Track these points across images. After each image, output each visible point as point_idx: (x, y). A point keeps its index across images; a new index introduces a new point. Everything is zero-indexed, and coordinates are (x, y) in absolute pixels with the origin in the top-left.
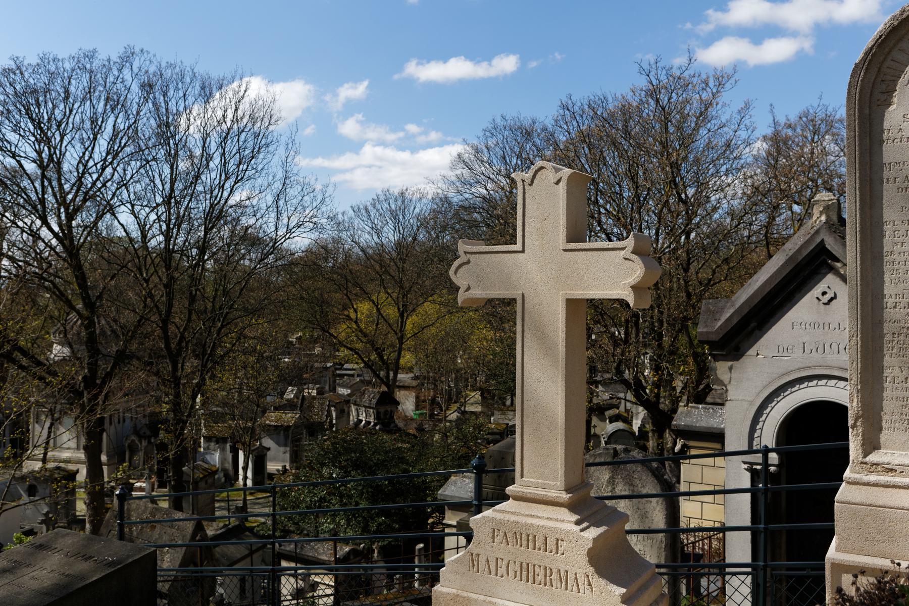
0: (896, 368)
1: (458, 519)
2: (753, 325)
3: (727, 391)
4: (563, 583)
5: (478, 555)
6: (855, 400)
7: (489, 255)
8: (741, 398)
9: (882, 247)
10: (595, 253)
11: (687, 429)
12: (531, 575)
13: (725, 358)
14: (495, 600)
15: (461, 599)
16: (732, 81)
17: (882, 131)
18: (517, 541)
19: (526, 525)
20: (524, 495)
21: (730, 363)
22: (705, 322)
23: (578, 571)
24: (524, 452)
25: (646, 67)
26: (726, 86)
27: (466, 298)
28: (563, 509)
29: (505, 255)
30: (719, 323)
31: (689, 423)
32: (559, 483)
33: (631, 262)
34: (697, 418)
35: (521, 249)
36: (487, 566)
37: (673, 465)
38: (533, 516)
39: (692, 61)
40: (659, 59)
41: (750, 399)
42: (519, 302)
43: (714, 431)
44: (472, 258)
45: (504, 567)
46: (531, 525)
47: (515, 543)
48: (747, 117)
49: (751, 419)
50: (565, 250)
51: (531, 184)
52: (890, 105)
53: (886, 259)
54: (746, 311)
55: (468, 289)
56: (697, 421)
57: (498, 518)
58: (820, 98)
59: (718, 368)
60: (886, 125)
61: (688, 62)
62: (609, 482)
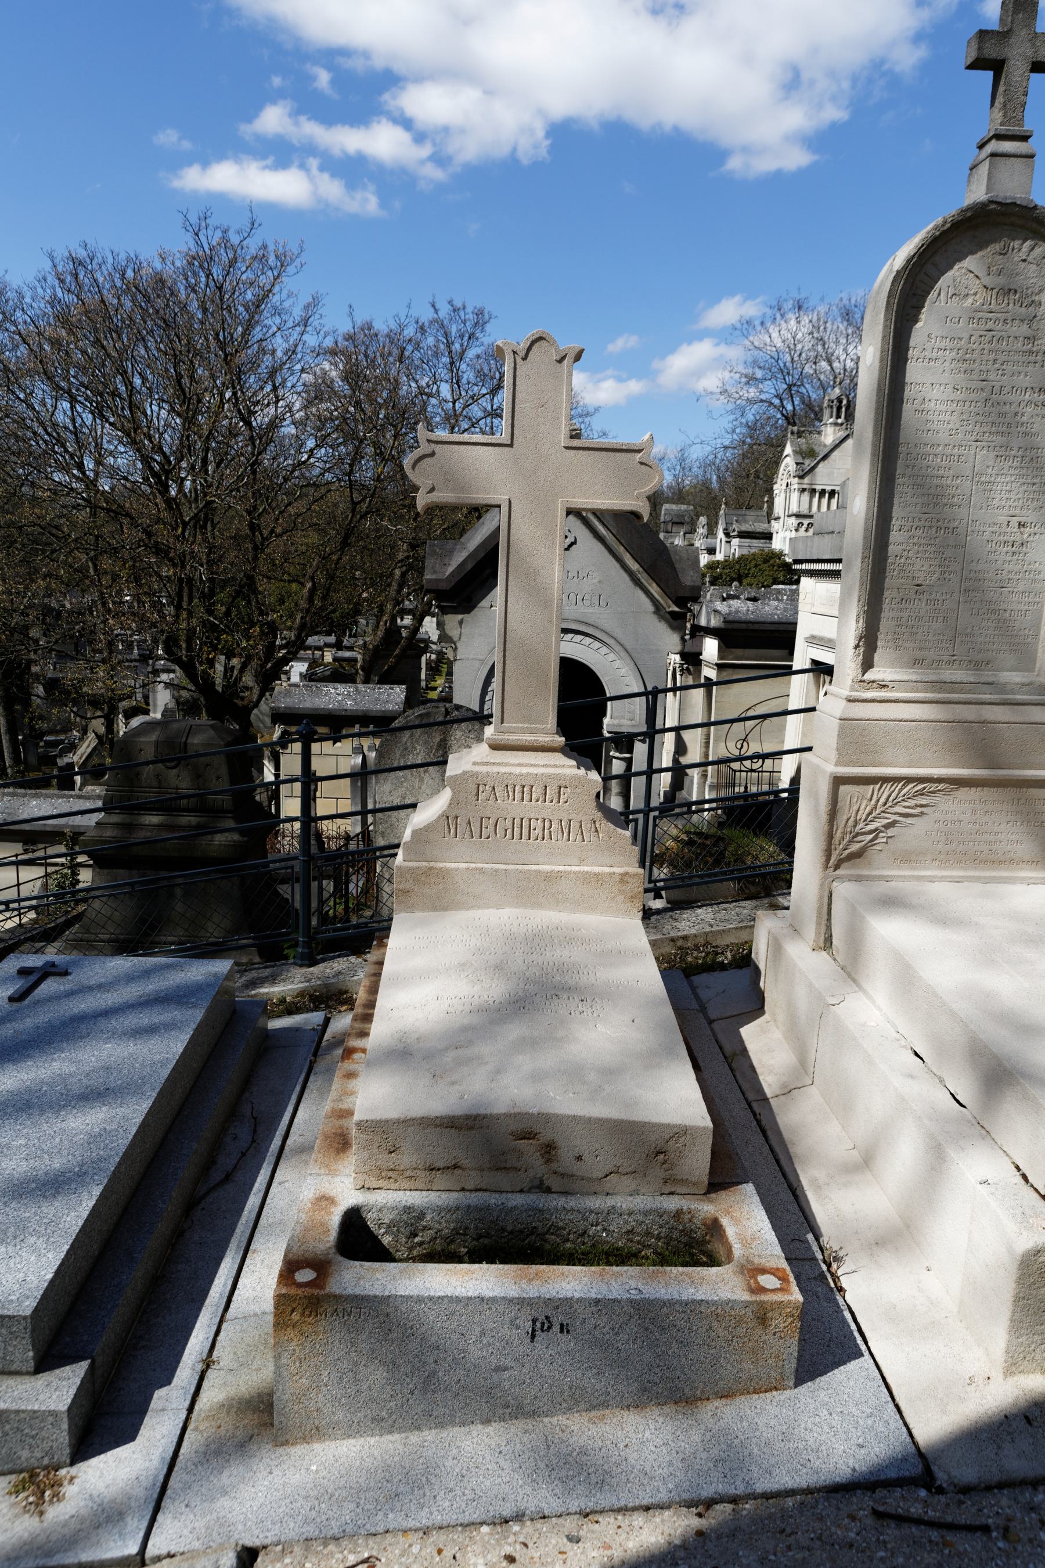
0: (895, 590)
4: (565, 834)
5: (457, 817)
6: (861, 621)
8: (471, 656)
9: (895, 470)
11: (288, 711)
13: (455, 611)
16: (297, 262)
17: (908, 349)
19: (521, 775)
20: (509, 742)
21: (460, 617)
23: (583, 819)
25: (194, 220)
27: (429, 500)
30: (450, 569)
31: (290, 705)
32: (549, 726)
35: (509, 442)
39: (256, 225)
40: (209, 214)
41: (481, 657)
42: (505, 509)
44: (438, 448)
45: (491, 827)
48: (317, 316)
50: (567, 448)
51: (524, 359)
52: (916, 321)
53: (898, 481)
58: (409, 307)
60: (912, 343)
61: (249, 225)
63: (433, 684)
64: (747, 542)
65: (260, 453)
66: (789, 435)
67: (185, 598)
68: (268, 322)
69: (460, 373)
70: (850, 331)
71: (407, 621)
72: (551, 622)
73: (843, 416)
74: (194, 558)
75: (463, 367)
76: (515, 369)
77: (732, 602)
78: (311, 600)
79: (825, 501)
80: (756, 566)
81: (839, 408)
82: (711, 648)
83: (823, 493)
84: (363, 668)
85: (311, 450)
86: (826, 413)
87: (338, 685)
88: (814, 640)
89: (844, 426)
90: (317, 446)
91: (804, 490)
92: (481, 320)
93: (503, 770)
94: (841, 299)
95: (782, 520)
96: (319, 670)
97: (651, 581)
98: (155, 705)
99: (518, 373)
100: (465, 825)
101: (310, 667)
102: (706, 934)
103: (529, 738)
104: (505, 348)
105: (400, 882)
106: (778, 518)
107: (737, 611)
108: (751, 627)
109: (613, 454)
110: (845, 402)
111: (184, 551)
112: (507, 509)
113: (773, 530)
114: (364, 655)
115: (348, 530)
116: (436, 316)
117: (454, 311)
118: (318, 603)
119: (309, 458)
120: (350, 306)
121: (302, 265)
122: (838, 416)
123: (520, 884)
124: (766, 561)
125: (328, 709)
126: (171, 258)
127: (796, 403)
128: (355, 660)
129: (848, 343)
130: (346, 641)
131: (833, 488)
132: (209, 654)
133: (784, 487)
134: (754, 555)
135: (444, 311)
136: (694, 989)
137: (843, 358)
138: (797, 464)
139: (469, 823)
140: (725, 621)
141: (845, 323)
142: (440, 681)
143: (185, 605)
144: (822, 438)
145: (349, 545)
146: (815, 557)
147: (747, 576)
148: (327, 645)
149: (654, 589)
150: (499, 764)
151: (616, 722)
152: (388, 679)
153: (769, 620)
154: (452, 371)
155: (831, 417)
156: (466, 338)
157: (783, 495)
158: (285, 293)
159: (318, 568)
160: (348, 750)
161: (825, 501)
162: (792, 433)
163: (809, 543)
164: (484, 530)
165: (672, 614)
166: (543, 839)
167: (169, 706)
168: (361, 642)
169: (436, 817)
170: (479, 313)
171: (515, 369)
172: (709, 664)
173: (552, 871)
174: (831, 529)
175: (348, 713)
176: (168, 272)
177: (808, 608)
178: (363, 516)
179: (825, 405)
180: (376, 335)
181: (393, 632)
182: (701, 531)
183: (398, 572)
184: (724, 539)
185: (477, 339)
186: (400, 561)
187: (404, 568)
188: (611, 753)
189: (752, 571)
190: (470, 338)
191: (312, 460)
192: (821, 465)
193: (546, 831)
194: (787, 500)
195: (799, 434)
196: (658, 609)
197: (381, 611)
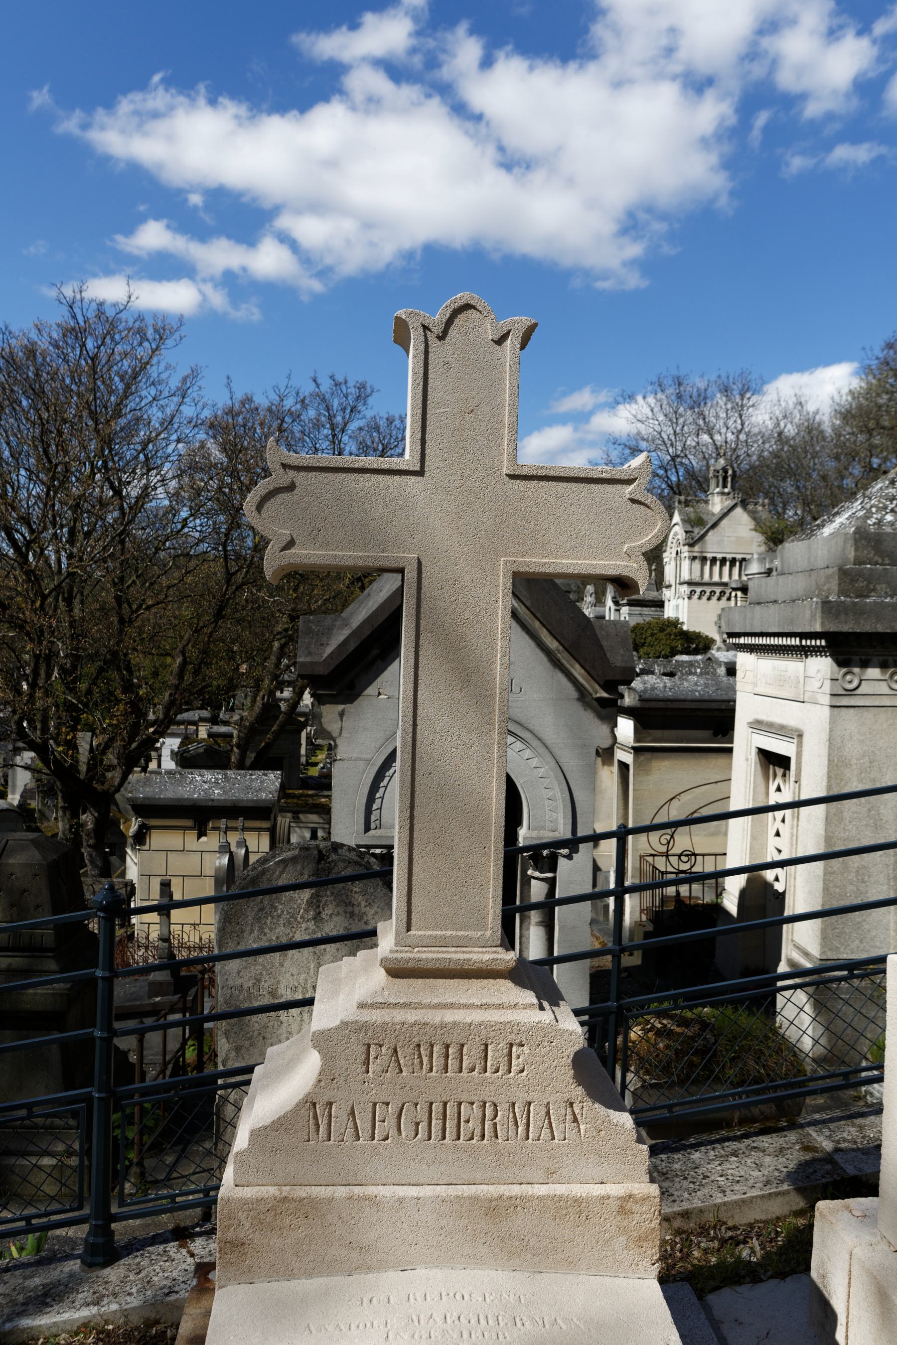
1: (310, 1044)
2: (375, 652)
3: (336, 746)
5: (330, 1104)
7: (341, 476)
8: (355, 756)
10: (573, 486)
11: (147, 802)
12: (450, 1125)
13: (334, 700)
14: (372, 1190)
15: (294, 1205)
16: (177, 336)
18: (421, 1063)
19: (443, 1026)
20: (422, 965)
21: (340, 707)
22: (307, 648)
23: (552, 1099)
24: (414, 878)
26: (167, 341)
27: (285, 562)
28: (502, 982)
29: (380, 477)
30: (329, 650)
31: (150, 795)
32: (488, 933)
33: (643, 508)
34: (160, 787)
36: (350, 1124)
37: (94, 854)
38: (501, 1006)
41: (368, 756)
42: (411, 575)
43: (185, 803)
44: (300, 478)
45: (391, 1120)
46: (455, 1024)
47: (417, 1067)
48: (196, 388)
49: (369, 785)
51: (442, 337)
54: (367, 633)
55: (291, 544)
56: (161, 791)
57: (380, 1020)
59: (324, 714)
62: (310, 903)
63: (313, 759)
64: (637, 609)
65: (130, 522)
66: (676, 504)
67: (43, 673)
68: (144, 393)
69: (342, 446)
70: (729, 406)
71: (287, 693)
72: (490, 759)
73: (729, 485)
74: (53, 632)
75: (345, 438)
76: (426, 353)
77: (646, 678)
78: (181, 675)
79: (716, 568)
80: (652, 635)
81: (725, 479)
82: (625, 728)
83: (714, 560)
84: (238, 746)
85: (185, 520)
86: (713, 483)
87: (205, 772)
88: (758, 725)
89: (731, 495)
90: (191, 515)
91: (694, 558)
92: (363, 393)
93: (411, 1016)
94: (719, 377)
95: (673, 588)
96: (192, 747)
97: (573, 661)
98: (14, 786)
99: (431, 360)
100: (344, 1117)
101: (182, 744)
102: (718, 1207)
103: (455, 956)
104: (410, 321)
105: (228, 1227)
106: (669, 586)
107: (653, 688)
108: (671, 705)
109: (587, 487)
110: (730, 472)
111: (42, 625)
112: (415, 574)
113: (665, 598)
114: (239, 731)
115: (222, 601)
116: (317, 390)
117: (336, 385)
118: (188, 678)
119: (183, 528)
120: (228, 378)
121: (181, 338)
122: (725, 486)
123: (443, 1222)
124: (662, 630)
125: (193, 800)
126: (47, 330)
127: (680, 474)
128: (230, 736)
129: (728, 418)
130: (222, 715)
131: (724, 555)
132: (66, 736)
133: (674, 555)
134: (649, 623)
135: (326, 386)
136: (708, 1310)
137: (723, 430)
138: (686, 532)
139: (352, 1113)
140: (641, 700)
141: (724, 398)
142: (321, 756)
143: (41, 683)
144: (710, 507)
145: (223, 617)
146: (757, 630)
147: (643, 645)
148: (202, 719)
149: (578, 672)
150: (404, 1006)
151: (535, 834)
152: (263, 763)
153: (690, 698)
154: (334, 443)
155: (718, 486)
156: (348, 411)
157: (673, 563)
158: (162, 367)
159: (189, 641)
160: (215, 846)
161: (716, 568)
162: (680, 502)
163: (749, 614)
164: (371, 603)
165: (600, 700)
166: (483, 1137)
167: (29, 787)
168: (236, 717)
169: (293, 1104)
170: (362, 387)
171: (426, 353)
172: (623, 747)
173: (500, 1198)
174: (773, 598)
175: (215, 804)
176: (43, 344)
177: (749, 688)
178: (239, 587)
179: (711, 475)
180: (257, 409)
181: (271, 708)
182: (589, 599)
183: (276, 644)
184: (613, 607)
185: (359, 412)
186: (278, 634)
187: (283, 641)
188: (530, 872)
189: (648, 640)
190: (352, 411)
191: (186, 530)
192: (710, 533)
193: (488, 1124)
194: (678, 568)
195: (687, 503)
196: (583, 695)
197: (257, 687)
